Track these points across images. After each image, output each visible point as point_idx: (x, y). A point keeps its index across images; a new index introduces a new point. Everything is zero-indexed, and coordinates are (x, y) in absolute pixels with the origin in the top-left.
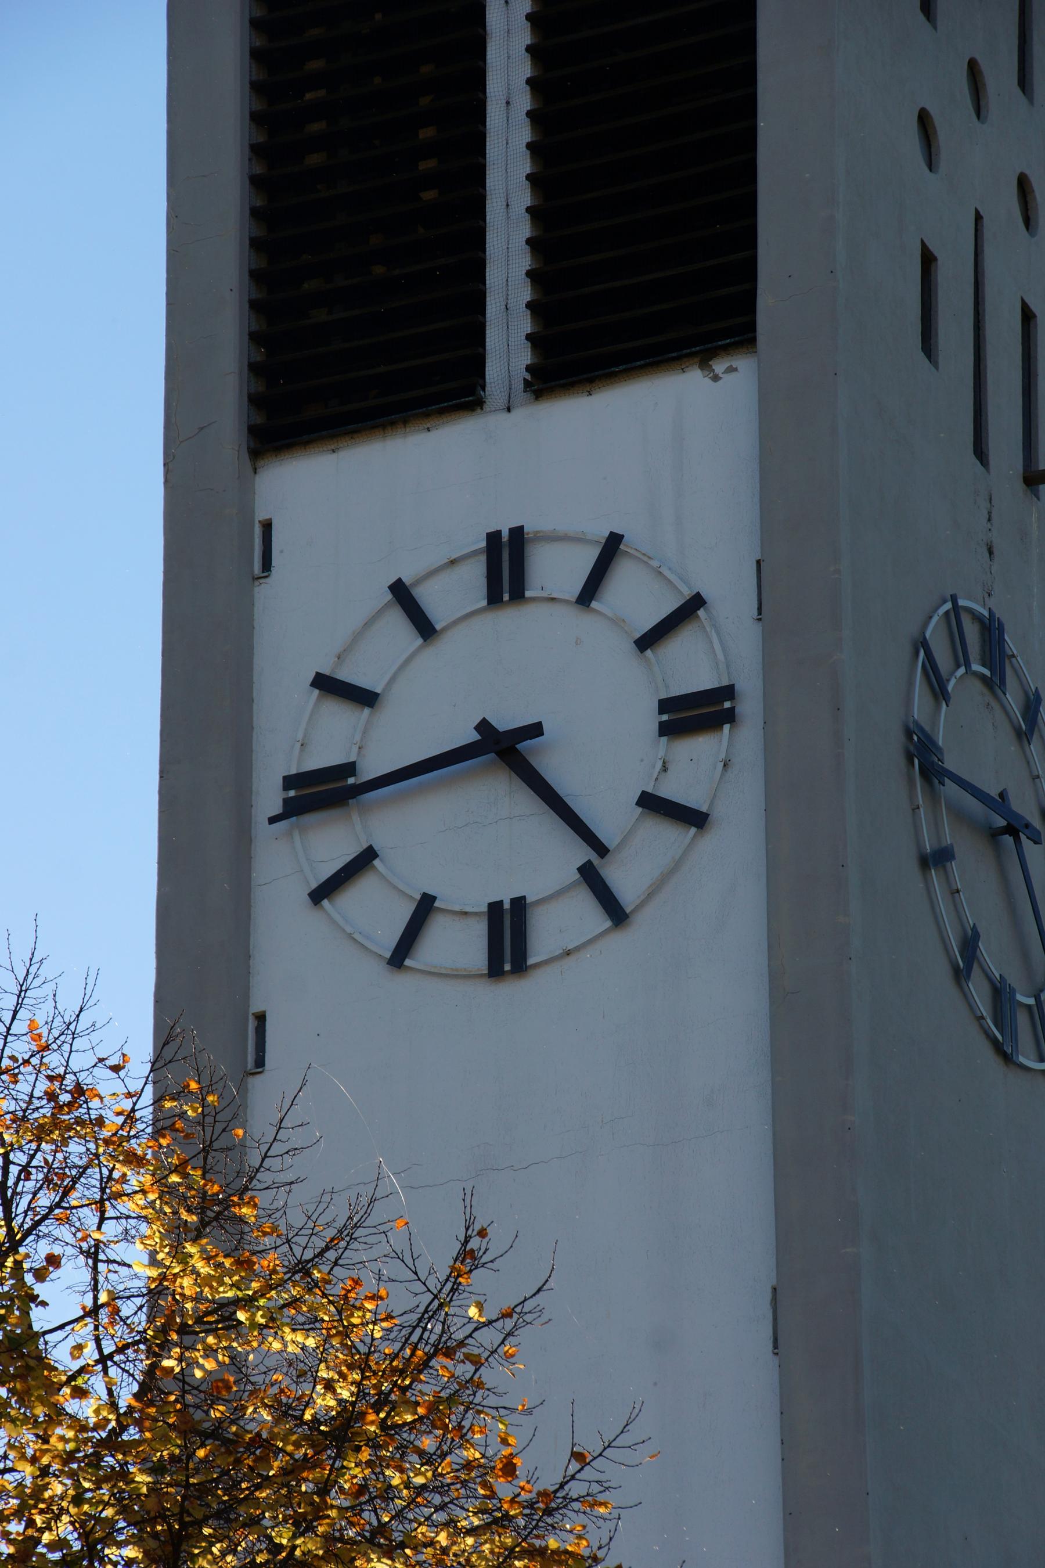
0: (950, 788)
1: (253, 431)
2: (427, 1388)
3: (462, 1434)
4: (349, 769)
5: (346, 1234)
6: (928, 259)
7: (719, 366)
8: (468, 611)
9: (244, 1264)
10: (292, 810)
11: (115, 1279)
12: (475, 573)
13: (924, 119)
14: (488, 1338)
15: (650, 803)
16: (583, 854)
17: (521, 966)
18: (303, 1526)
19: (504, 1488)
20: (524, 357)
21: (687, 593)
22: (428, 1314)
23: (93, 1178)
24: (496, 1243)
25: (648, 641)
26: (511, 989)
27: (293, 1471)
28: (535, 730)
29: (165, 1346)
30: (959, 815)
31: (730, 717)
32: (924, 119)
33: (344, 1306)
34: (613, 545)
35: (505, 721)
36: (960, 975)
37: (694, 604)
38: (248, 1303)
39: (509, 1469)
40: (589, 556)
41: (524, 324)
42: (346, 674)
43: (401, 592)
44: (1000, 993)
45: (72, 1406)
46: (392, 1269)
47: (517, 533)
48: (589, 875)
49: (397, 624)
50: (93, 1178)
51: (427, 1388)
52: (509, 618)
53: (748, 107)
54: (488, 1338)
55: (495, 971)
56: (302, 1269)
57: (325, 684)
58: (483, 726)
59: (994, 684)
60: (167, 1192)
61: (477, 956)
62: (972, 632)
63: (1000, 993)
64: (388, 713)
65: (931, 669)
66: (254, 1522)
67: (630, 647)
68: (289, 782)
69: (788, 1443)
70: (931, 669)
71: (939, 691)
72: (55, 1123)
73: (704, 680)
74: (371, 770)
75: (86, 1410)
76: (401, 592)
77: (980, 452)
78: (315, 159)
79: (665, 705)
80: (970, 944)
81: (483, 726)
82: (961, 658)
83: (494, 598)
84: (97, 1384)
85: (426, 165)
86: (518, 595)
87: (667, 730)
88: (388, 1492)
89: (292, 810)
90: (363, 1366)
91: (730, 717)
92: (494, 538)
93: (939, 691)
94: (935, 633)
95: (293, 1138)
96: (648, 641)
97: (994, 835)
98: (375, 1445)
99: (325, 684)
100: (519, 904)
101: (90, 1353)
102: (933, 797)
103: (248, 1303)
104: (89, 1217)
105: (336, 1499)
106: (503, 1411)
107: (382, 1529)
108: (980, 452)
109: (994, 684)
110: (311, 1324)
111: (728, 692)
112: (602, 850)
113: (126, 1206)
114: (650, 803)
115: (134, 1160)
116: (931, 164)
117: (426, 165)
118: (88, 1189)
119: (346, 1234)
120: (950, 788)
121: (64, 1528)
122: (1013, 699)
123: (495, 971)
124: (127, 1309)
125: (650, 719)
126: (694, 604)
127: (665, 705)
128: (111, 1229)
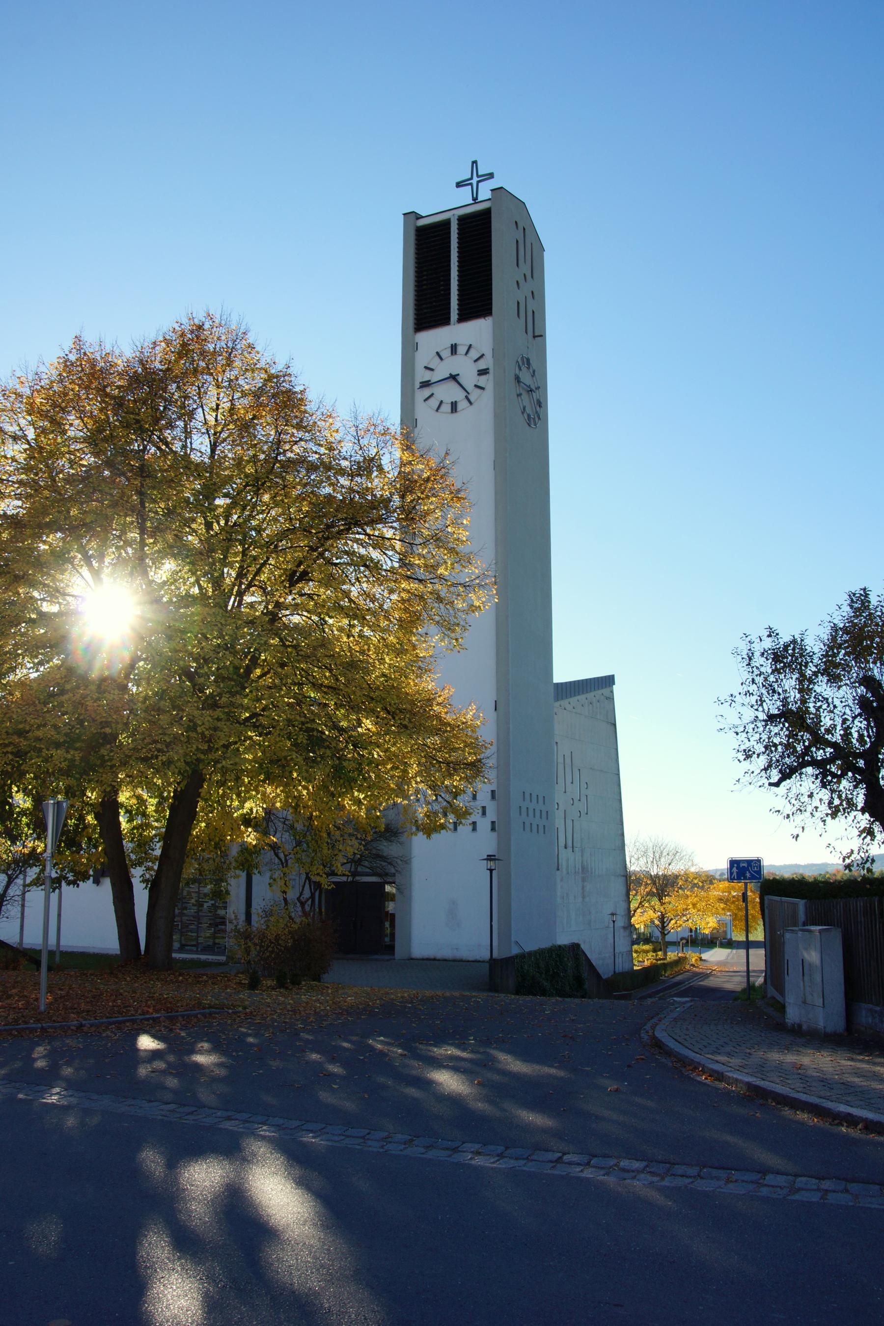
0: (522, 384)
1: (415, 328)
2: (441, 473)
3: (446, 481)
4: (430, 381)
5: (428, 451)
6: (518, 303)
7: (487, 318)
8: (513, 932)
9: (413, 455)
10: (421, 387)
11: (395, 457)
12: (450, 350)
13: (517, 282)
14: (450, 466)
15: (476, 386)
16: (466, 394)
17: (456, 411)
18: (422, 493)
19: (452, 488)
20: (457, 317)
21: (482, 353)
22: (441, 462)
23: (390, 442)
24: (451, 451)
25: (476, 361)
26: (455, 415)
27: (421, 485)
28: (458, 375)
29: (401, 467)
30: (523, 388)
31: (488, 373)
32: (517, 282)
33: (428, 461)
34: (470, 346)
35: (453, 374)
36: (523, 413)
37: (483, 355)
38: (414, 461)
39: (453, 485)
40: (467, 348)
41: (457, 312)
42: (429, 366)
43: (438, 353)
44: (529, 416)
45: (388, 475)
46: (435, 455)
47: (456, 344)
48: (467, 397)
49: (437, 358)
50: (390, 442)
51: (441, 473)
52: (454, 357)
53: (490, 260)
54: (450, 466)
55: (452, 412)
56: (422, 456)
57: (426, 368)
58: (450, 374)
59: (528, 368)
60: (401, 444)
61: (450, 410)
62: (525, 360)
63: (529, 416)
64: (435, 372)
65: (519, 365)
66: (415, 493)
67: (473, 362)
68: (421, 383)
69: (496, 483)
70: (519, 365)
71: (520, 369)
72: (384, 433)
73: (484, 367)
74: (432, 381)
75: (390, 476)
76: (438, 353)
77: (526, 332)
78: (425, 287)
79: (478, 371)
80: (524, 408)
81: (450, 374)
82: (523, 364)
83: (452, 354)
84: (392, 472)
85: (442, 288)
86: (456, 353)
87: (478, 375)
88: (435, 488)
89: (421, 387)
90: (431, 470)
91: (488, 373)
92: (452, 345)
93: (520, 369)
94: (519, 360)
95: (420, 436)
96: (476, 361)
97: (528, 391)
98: (433, 481)
99: (426, 368)
100: (456, 402)
101: (390, 468)
102: (519, 386)
103: (414, 461)
104: (390, 448)
105: (427, 489)
106: (452, 477)
107: (434, 494)
108: (526, 332)
109: (528, 368)
110: (423, 464)
111: (488, 369)
112: (468, 393)
113: (395, 446)
114: (476, 386)
115: (396, 439)
116: (519, 288)
117: (442, 288)
118: (390, 443)
119: (428, 451)
120: (522, 384)
121: (387, 493)
122: (531, 371)
123: (452, 412)
124: (396, 461)
125: (476, 373)
126: (483, 355)
127: (478, 371)
128: (393, 449)
